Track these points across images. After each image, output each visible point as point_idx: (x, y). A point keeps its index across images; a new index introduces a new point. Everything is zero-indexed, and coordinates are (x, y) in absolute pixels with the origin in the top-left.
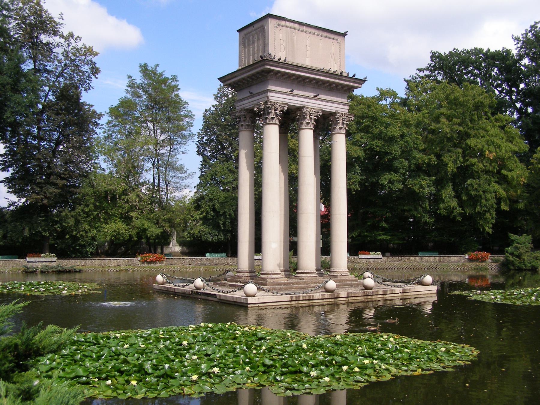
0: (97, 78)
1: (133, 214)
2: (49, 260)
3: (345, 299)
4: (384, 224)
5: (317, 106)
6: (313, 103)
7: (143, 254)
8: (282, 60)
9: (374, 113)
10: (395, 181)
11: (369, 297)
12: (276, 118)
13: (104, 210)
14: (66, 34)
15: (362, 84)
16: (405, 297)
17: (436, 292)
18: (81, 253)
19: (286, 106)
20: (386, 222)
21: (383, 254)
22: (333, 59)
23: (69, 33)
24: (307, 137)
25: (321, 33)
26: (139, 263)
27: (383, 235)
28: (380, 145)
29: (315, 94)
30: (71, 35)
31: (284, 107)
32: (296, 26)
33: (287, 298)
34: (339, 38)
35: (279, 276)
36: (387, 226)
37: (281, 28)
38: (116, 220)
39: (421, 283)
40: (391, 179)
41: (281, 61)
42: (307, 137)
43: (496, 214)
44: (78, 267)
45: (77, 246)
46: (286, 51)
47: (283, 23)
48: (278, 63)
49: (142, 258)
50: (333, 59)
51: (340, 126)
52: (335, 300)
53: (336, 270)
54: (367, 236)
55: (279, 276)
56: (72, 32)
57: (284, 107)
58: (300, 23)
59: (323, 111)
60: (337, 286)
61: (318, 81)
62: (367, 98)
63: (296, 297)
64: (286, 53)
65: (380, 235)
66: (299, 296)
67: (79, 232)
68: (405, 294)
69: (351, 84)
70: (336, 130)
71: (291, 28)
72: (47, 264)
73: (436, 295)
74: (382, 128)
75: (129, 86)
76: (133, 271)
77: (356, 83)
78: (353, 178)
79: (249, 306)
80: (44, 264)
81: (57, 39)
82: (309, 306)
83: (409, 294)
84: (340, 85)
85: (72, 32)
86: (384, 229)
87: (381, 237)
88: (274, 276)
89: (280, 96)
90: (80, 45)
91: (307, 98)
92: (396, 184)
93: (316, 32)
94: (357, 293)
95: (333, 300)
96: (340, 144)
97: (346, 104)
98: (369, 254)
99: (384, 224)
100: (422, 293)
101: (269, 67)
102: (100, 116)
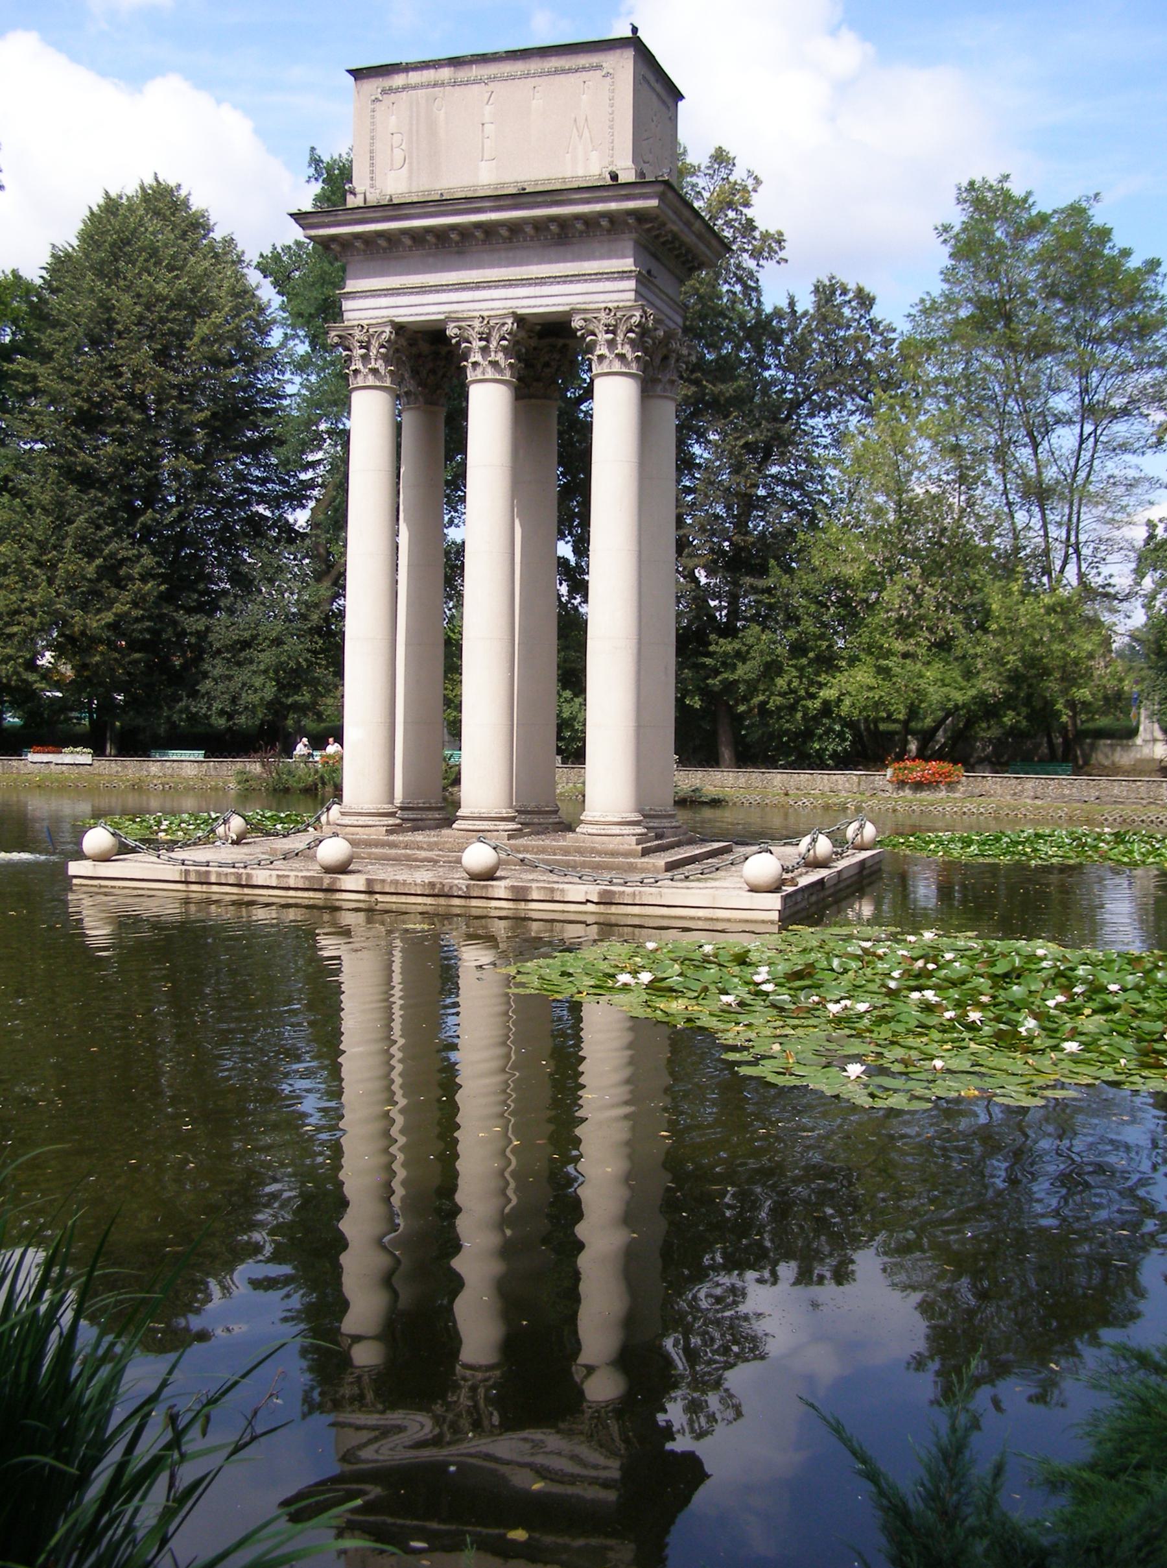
6: (481, 299)
11: (456, 901)
16: (613, 920)
17: (775, 916)
22: (586, 133)
24: (489, 407)
25: (534, 65)
26: (889, 787)
32: (446, 73)
42: (489, 407)
46: (411, 163)
47: (399, 80)
58: (455, 62)
61: (488, 229)
63: (197, 872)
66: (208, 873)
68: (614, 909)
69: (613, 206)
71: (428, 86)
77: (628, 198)
79: (75, 881)
91: (471, 289)
93: (519, 67)
94: (404, 883)
96: (614, 406)
97: (623, 275)
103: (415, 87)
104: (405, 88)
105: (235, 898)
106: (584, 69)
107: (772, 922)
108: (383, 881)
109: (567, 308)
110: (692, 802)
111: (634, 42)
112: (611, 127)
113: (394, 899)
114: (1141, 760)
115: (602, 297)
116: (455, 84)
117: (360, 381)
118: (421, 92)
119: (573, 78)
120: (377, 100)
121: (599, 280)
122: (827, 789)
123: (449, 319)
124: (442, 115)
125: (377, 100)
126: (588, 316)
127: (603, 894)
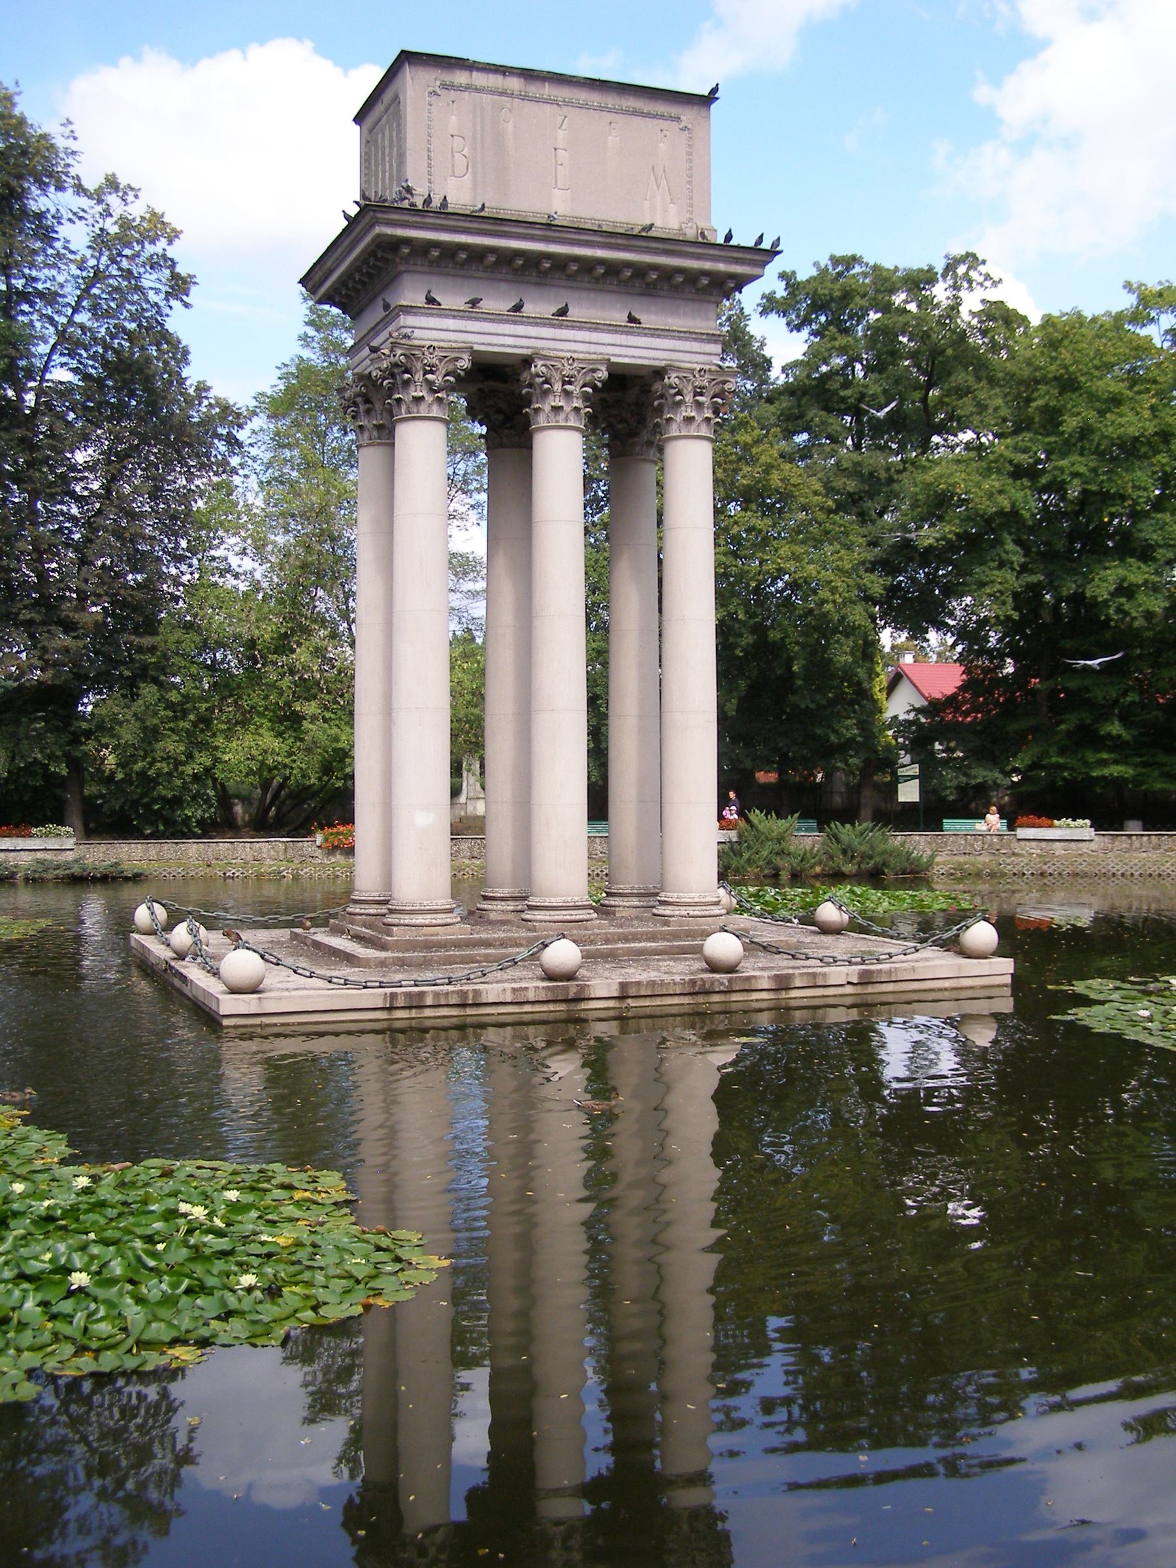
0: (187, 305)
1: (310, 708)
2: (53, 844)
3: (611, 1004)
4: (1115, 728)
5: (593, 348)
6: (580, 339)
7: (331, 825)
9: (1066, 367)
10: (1139, 586)
11: (716, 998)
12: (429, 398)
13: (231, 695)
14: (91, 184)
15: (764, 264)
16: (870, 1000)
17: (1008, 980)
18: (169, 822)
19: (466, 356)
20: (1124, 719)
21: (1098, 826)
22: (664, 183)
23: (107, 179)
25: (612, 100)
27: (1116, 762)
28: (1082, 469)
29: (554, 310)
30: (112, 184)
31: (457, 359)
32: (514, 83)
33: (374, 997)
34: (688, 115)
35: (441, 918)
36: (1126, 736)
38: (261, 726)
39: (953, 945)
40: (1124, 579)
44: (129, 868)
45: (155, 801)
46: (474, 174)
47: (461, 77)
48: (444, 215)
49: (326, 840)
50: (664, 183)
52: (573, 1006)
53: (671, 896)
54: (1063, 767)
55: (441, 918)
56: (114, 175)
57: (457, 359)
58: (527, 74)
59: (611, 366)
60: (586, 956)
61: (587, 265)
62: (1094, 320)
65: (1103, 763)
66: (422, 994)
67: (151, 764)
68: (870, 989)
69: (722, 267)
71: (492, 92)
72: (48, 856)
73: (1008, 991)
74: (1091, 416)
75: (311, 323)
76: (296, 878)
77: (737, 261)
78: (992, 582)
79: (225, 1022)
80: (39, 855)
81: (68, 200)
82: (461, 1028)
83: (890, 987)
84: (701, 275)
85: (114, 175)
86: (1116, 745)
87: (1106, 772)
88: (419, 920)
89: (446, 325)
90: (136, 210)
92: (1141, 598)
95: (562, 1007)
98: (1051, 826)
99: (1115, 728)
100: (947, 984)
101: (389, 231)
102: (236, 418)
103: (477, 90)
104: (468, 88)
105: (454, 1021)
106: (662, 117)
107: (1006, 985)
108: (639, 983)
109: (663, 364)
110: (114, 879)
111: (406, 58)
112: (690, 183)
113: (647, 1002)
114: (467, 818)
115: (688, 357)
116: (524, 98)
117: (423, 410)
118: (487, 98)
120: (435, 93)
121: (687, 339)
122: (250, 858)
125: (435, 93)
127: (863, 974)
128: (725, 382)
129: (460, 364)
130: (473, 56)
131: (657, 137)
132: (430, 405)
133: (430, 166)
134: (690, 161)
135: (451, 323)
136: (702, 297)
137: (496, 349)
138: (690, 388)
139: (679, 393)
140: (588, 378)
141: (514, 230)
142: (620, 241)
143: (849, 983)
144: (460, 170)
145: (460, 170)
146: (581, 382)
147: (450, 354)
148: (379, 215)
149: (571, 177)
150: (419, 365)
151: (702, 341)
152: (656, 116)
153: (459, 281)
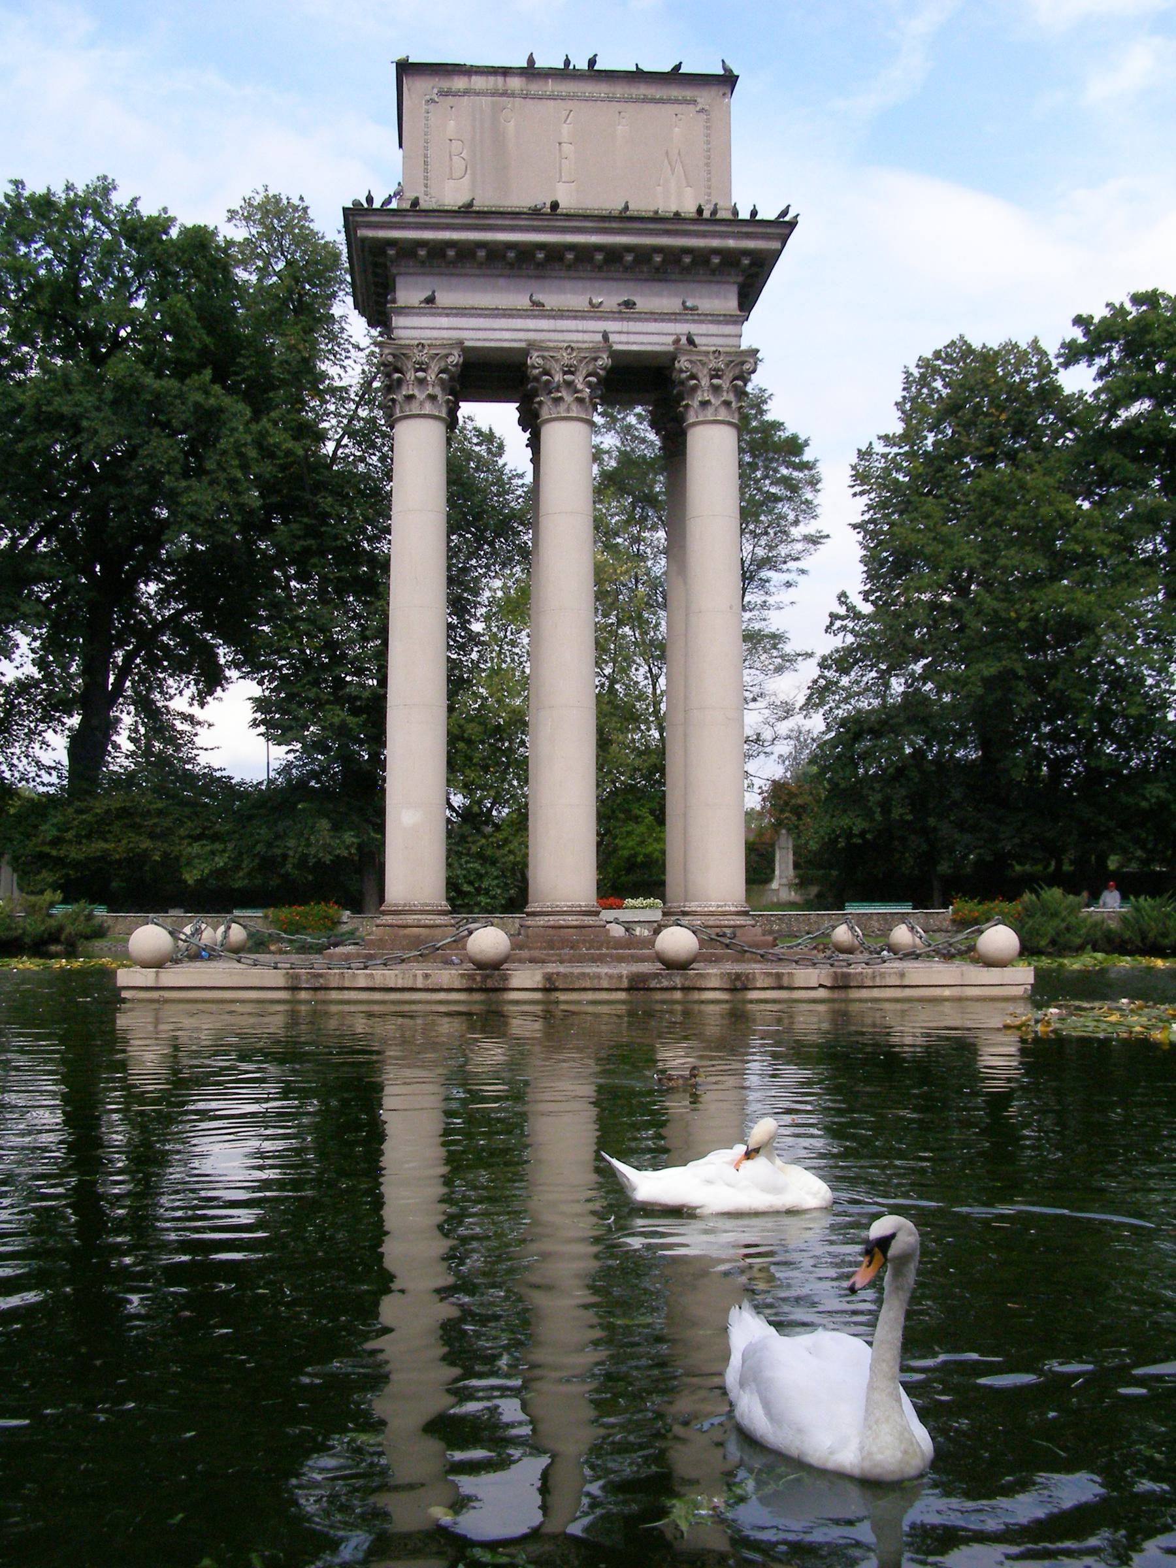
5: (435, 334)
6: (570, 325)
8: (744, 214)
22: (679, 168)
31: (447, 356)
32: (515, 83)
34: (704, 97)
37: (450, 100)
41: (718, 216)
43: (154, 702)
46: (474, 174)
47: (460, 83)
50: (679, 168)
51: (703, 395)
53: (692, 906)
57: (447, 356)
59: (466, 351)
64: (473, 182)
69: (731, 243)
70: (692, 413)
100: (947, 992)
103: (478, 94)
104: (467, 92)
117: (414, 408)
118: (485, 101)
119: (671, 109)
123: (532, 345)
124: (511, 127)
126: (694, 358)
128: (743, 363)
129: (450, 360)
130: (469, 62)
131: (675, 123)
132: (422, 404)
133: (426, 171)
134: (708, 143)
135: (444, 321)
136: (719, 278)
137: (493, 344)
138: (705, 371)
139: (693, 377)
140: (591, 367)
141: (499, 222)
142: (614, 225)
143: (821, 986)
144: (458, 173)
145: (458, 173)
146: (584, 373)
147: (439, 350)
148: (359, 219)
149: (579, 168)
150: (410, 365)
151: (719, 322)
152: (669, 101)
153: (454, 280)
